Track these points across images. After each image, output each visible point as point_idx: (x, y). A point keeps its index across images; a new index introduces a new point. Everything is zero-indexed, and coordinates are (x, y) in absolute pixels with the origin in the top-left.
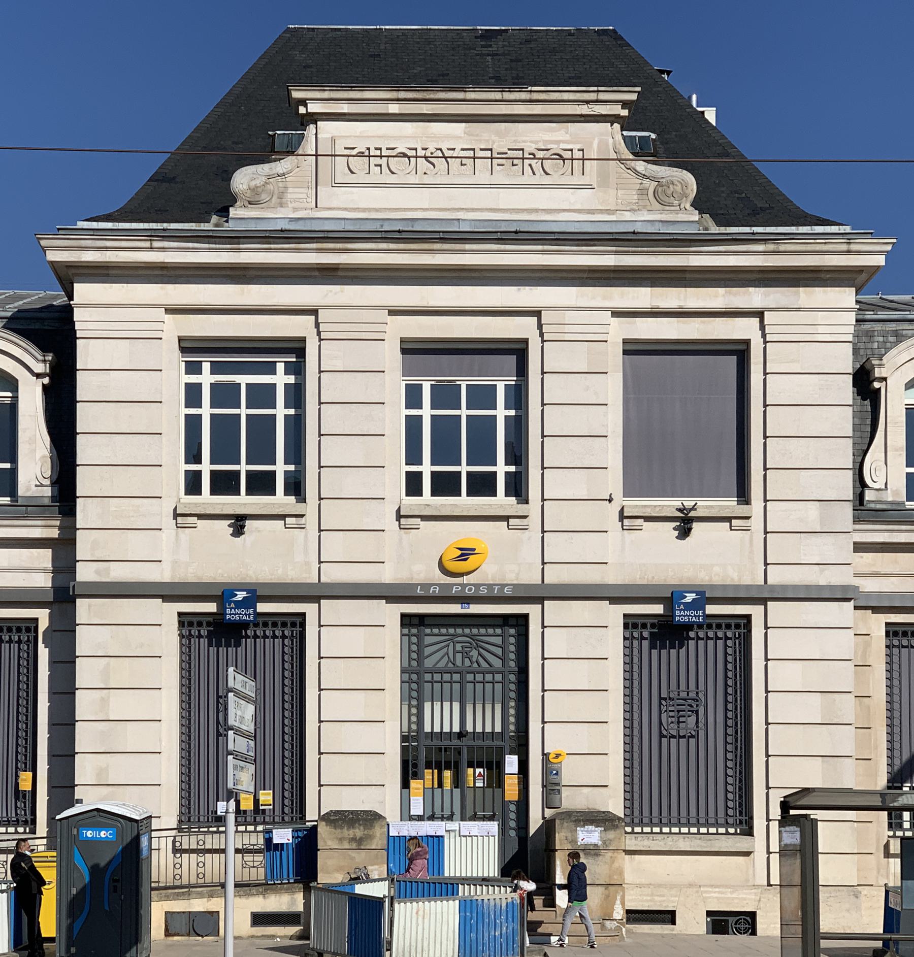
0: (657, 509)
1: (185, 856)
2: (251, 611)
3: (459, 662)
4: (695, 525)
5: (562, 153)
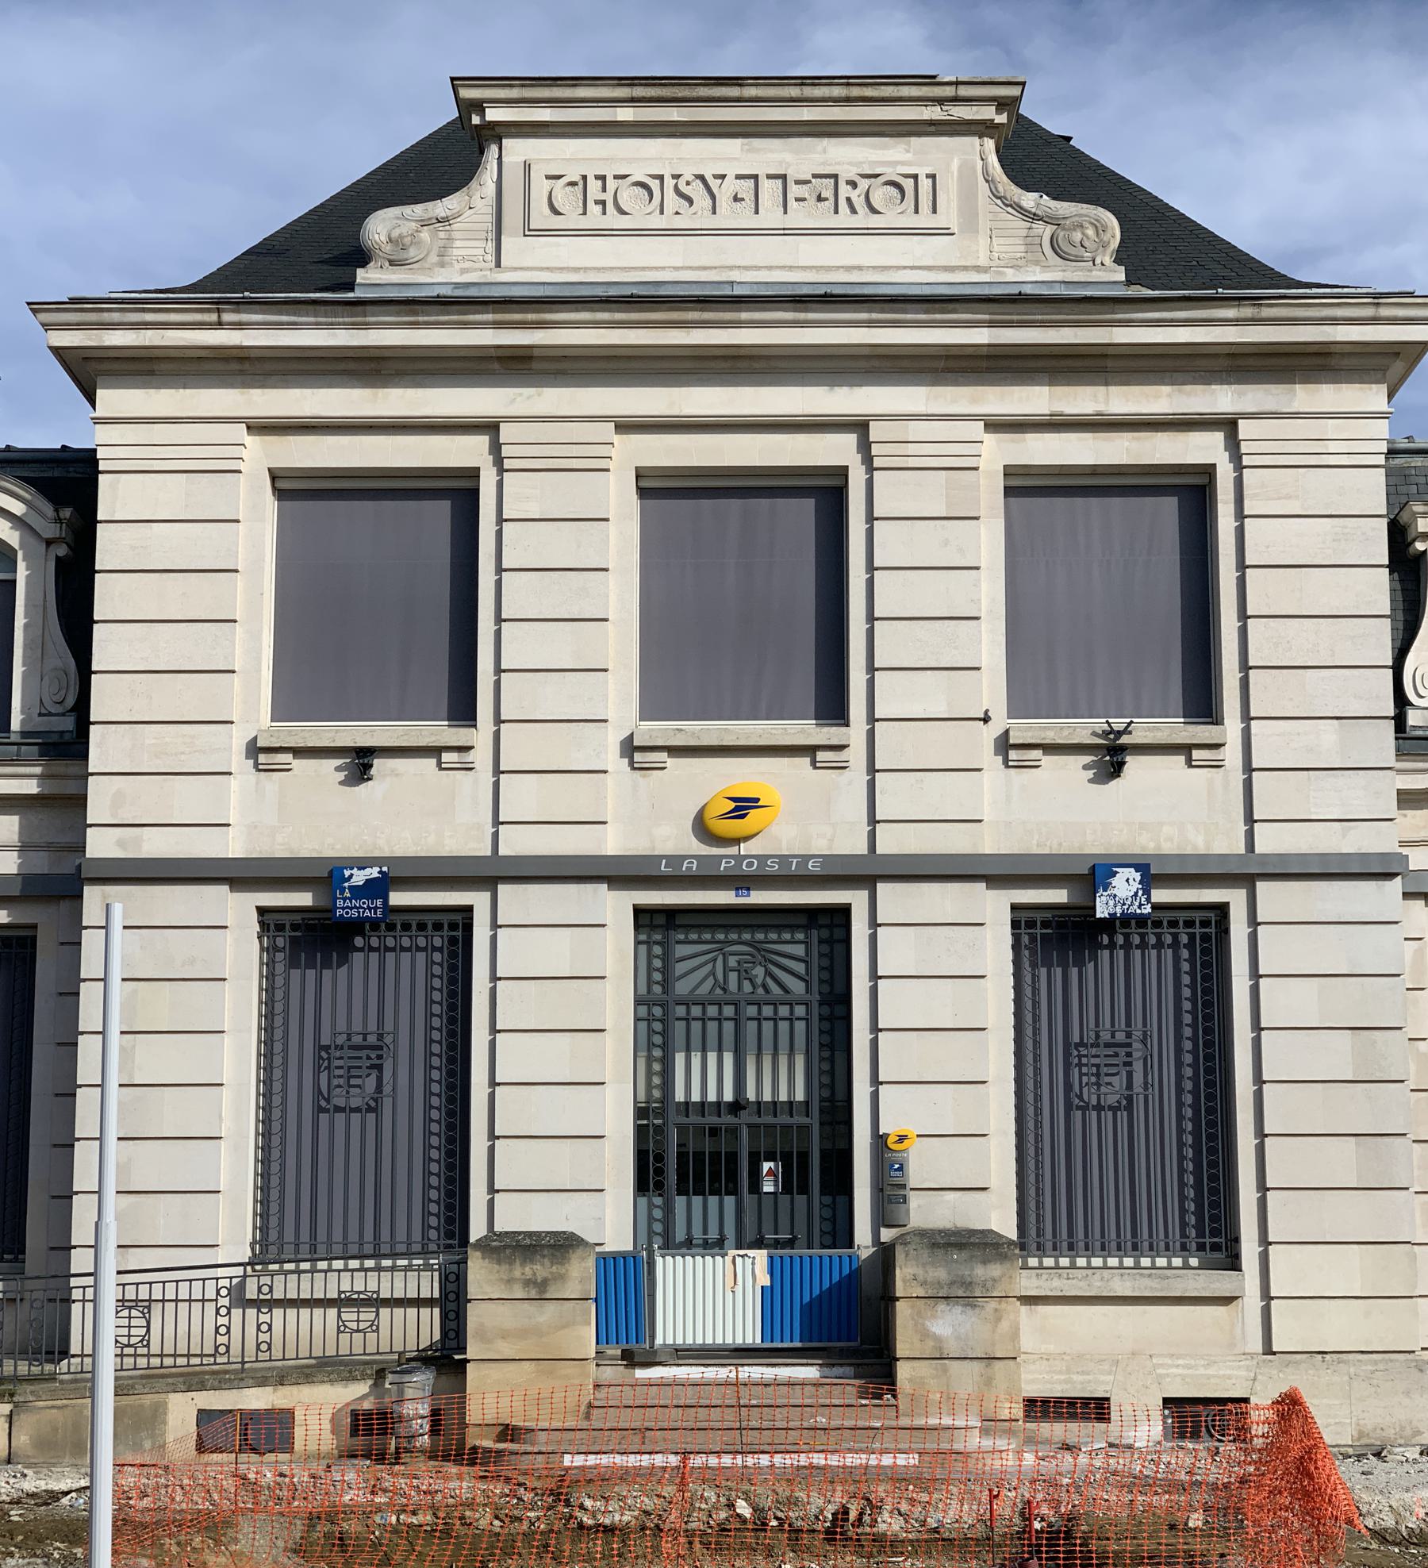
0: (1065, 733)
1: (278, 1313)
2: (379, 902)
3: (733, 985)
4: (1132, 763)
5: (900, 180)
